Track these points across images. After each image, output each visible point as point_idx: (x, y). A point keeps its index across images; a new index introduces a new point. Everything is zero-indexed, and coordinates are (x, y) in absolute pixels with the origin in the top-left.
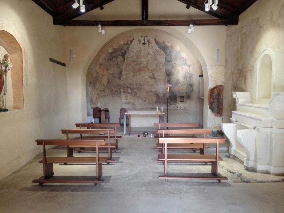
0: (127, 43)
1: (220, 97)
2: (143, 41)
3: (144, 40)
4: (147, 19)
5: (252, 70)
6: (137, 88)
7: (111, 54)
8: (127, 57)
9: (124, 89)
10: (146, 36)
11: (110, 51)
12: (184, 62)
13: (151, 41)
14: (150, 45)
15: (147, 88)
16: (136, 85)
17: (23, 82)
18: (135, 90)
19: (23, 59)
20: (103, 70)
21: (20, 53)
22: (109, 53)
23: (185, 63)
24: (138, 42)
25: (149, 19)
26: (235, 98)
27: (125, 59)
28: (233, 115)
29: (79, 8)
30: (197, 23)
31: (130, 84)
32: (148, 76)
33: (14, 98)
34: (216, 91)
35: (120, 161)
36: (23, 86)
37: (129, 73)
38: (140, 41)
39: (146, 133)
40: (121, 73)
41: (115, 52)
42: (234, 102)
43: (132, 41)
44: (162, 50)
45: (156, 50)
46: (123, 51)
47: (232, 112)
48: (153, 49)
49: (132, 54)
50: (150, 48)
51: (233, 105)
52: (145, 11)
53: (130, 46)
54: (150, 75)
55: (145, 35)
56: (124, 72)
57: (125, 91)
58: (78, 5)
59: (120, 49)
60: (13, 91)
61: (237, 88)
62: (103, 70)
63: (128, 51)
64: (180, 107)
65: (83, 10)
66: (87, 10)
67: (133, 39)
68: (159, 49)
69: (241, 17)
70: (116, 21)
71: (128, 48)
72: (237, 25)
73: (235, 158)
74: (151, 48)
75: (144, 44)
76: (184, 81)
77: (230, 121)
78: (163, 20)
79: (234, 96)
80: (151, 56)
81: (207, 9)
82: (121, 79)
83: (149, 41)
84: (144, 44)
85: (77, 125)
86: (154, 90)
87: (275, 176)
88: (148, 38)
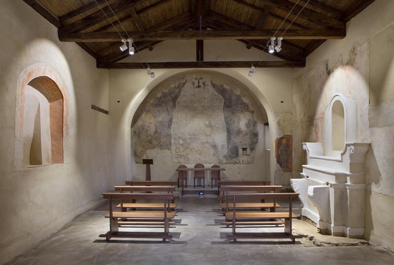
0: (178, 86)
1: (289, 148)
2: (198, 84)
3: (199, 82)
4: (203, 60)
5: (322, 118)
6: (190, 139)
7: (160, 98)
8: (179, 103)
9: (175, 140)
10: (201, 79)
11: (159, 95)
12: (246, 107)
13: (206, 83)
14: (206, 88)
15: (203, 138)
16: (189, 135)
17: (63, 132)
18: (188, 141)
19: (64, 106)
20: (150, 117)
21: (61, 100)
22: (158, 98)
23: (247, 109)
24: (192, 85)
25: (205, 60)
26: (305, 150)
27: (176, 104)
28: (303, 169)
29: (127, 51)
30: (257, 65)
31: (182, 134)
32: (204, 124)
33: (52, 151)
34: (284, 141)
35: (182, 223)
36: (63, 136)
37: (180, 121)
38: (193, 84)
39: (202, 193)
40: (171, 121)
41: (164, 97)
42: (305, 153)
43: (184, 84)
44: (220, 94)
45: (213, 93)
46: (173, 95)
47: (303, 166)
48: (209, 93)
49: (184, 98)
50: (205, 92)
51: (303, 158)
52: (200, 52)
53: (182, 90)
54: (206, 123)
55: (199, 77)
56: (174, 120)
57: (176, 142)
58: (127, 48)
59: (170, 93)
60: (52, 143)
61: (307, 139)
62: (150, 117)
63: (179, 95)
64: (243, 161)
65: (132, 53)
66: (136, 52)
67: (186, 82)
68: (217, 93)
69: (308, 59)
70: (167, 63)
71: (179, 92)
72: (305, 68)
73: (305, 218)
74: (207, 92)
75: (199, 86)
76: (247, 130)
77: (301, 177)
78: (221, 62)
79: (304, 147)
80: (206, 101)
81: (271, 51)
82: (172, 127)
83: (204, 84)
84: (199, 86)
85: (128, 183)
86: (211, 141)
87: (338, 227)
88: (203, 80)
